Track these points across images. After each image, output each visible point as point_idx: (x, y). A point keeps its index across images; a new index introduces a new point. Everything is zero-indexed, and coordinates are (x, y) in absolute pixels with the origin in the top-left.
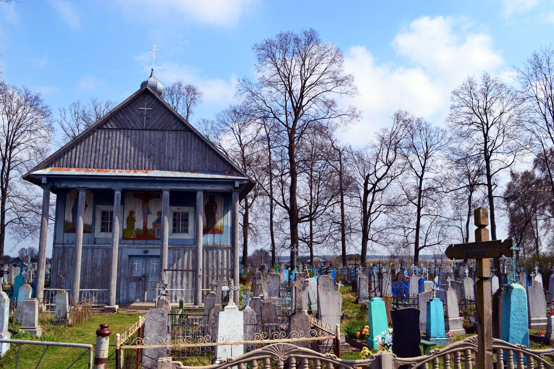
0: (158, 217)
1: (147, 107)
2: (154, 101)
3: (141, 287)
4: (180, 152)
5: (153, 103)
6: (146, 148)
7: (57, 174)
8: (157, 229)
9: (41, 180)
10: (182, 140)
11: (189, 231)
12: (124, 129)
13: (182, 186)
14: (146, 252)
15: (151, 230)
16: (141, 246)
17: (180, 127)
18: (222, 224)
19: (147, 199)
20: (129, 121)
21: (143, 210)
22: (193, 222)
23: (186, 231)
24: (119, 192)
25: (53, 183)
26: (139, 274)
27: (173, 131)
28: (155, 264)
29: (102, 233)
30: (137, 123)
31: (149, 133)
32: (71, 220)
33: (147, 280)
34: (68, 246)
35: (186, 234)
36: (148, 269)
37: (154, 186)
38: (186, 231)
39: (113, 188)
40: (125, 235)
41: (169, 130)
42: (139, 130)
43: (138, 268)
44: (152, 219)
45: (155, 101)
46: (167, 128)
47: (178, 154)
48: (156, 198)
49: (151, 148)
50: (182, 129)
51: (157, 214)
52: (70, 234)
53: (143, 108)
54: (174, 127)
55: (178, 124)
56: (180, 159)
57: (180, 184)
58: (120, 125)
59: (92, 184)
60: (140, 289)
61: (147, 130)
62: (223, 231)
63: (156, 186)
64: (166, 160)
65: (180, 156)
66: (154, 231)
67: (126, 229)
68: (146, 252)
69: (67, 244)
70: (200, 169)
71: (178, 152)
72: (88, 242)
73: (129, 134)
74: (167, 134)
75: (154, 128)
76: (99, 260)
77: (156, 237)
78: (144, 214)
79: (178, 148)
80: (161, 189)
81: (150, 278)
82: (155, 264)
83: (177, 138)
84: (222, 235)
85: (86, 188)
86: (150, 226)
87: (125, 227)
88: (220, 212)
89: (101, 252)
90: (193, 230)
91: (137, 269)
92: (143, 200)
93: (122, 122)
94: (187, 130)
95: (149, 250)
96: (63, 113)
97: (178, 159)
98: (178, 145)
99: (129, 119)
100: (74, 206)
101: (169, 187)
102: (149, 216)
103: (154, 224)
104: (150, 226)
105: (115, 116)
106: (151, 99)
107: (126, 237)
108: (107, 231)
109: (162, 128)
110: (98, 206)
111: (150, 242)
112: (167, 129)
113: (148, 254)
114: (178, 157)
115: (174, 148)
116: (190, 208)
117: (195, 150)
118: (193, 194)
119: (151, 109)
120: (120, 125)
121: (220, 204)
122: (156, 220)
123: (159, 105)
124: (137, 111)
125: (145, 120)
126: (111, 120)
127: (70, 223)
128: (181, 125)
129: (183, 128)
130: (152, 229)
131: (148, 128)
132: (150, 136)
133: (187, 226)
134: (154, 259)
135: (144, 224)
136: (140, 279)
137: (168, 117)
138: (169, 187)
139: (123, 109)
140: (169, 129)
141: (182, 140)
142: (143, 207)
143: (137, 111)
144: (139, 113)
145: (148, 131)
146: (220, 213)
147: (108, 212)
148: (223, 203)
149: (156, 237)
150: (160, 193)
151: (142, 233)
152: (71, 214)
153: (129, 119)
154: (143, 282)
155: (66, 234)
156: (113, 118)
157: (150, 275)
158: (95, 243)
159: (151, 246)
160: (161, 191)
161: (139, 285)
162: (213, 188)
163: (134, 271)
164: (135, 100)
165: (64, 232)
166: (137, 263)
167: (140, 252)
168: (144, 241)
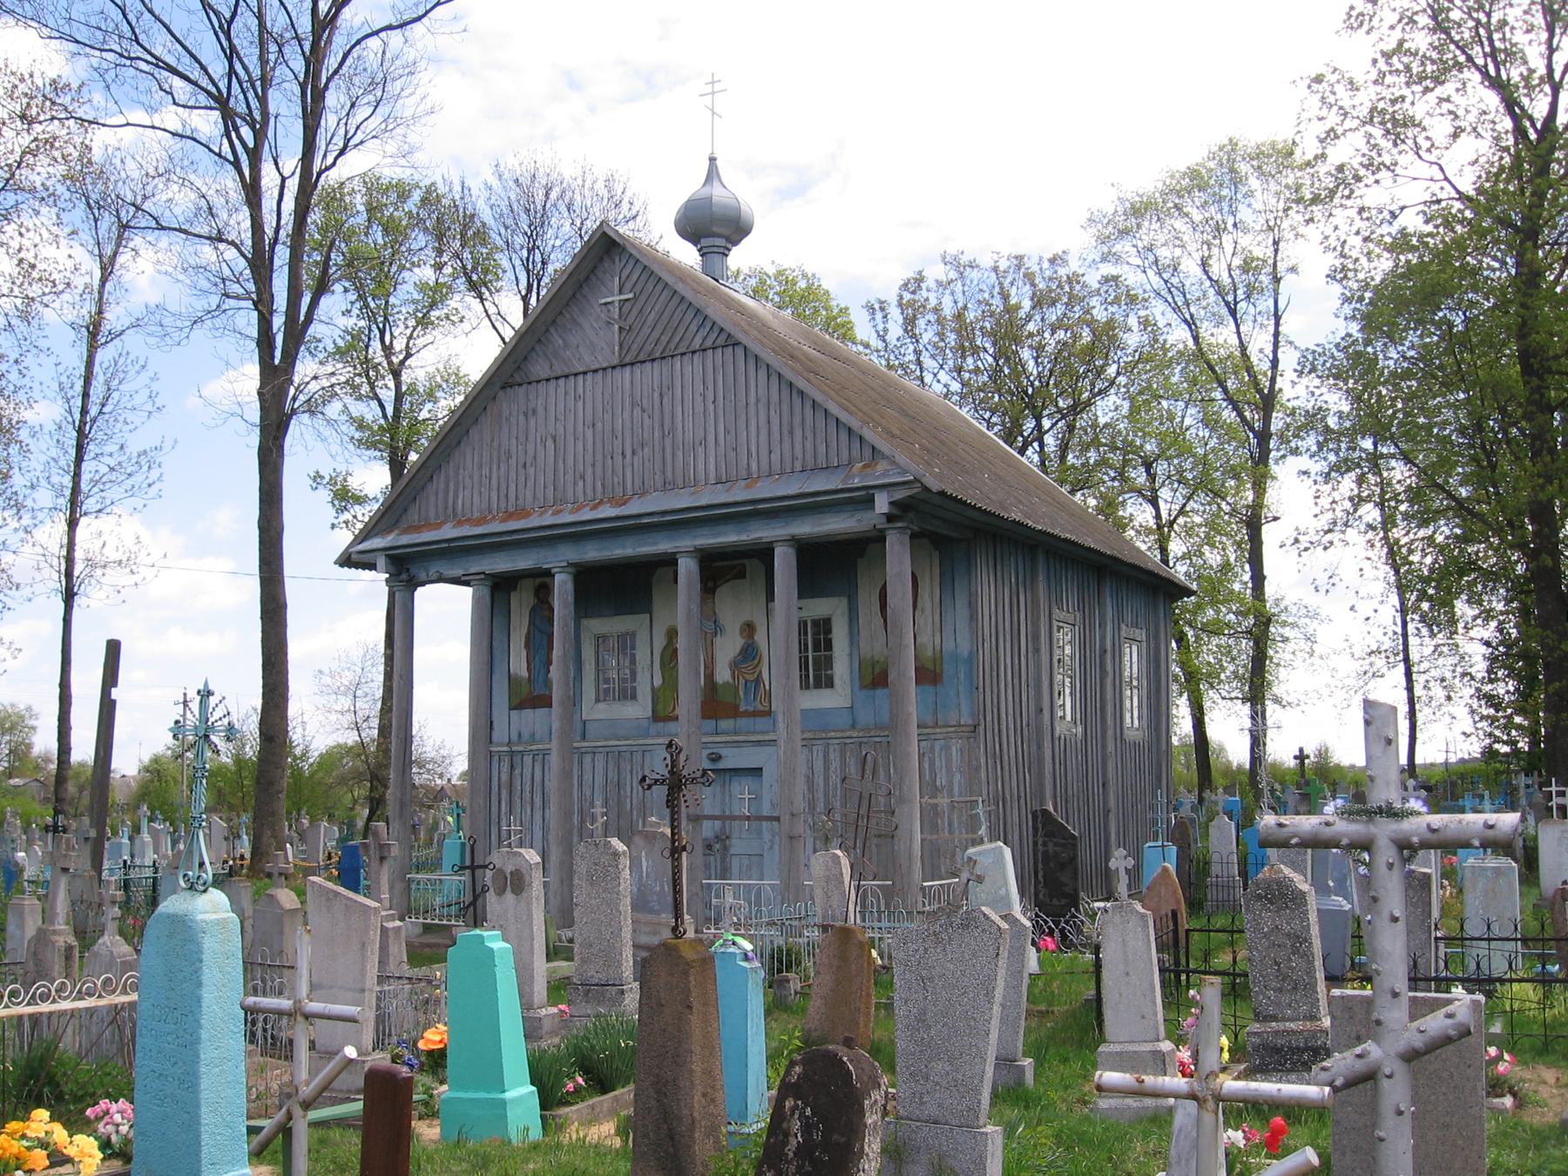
0: (743, 641)
8: (742, 681)
11: (837, 681)
14: (715, 758)
18: (938, 648)
22: (847, 651)
23: (830, 684)
28: (747, 796)
29: (601, 706)
34: (521, 748)
35: (825, 692)
37: (651, 545)
38: (830, 684)
39: (545, 566)
40: (660, 707)
48: (734, 578)
51: (742, 632)
53: (609, 300)
63: (656, 544)
67: (659, 689)
75: (641, 358)
77: (742, 708)
81: (734, 841)
82: (747, 796)
86: (723, 675)
87: (658, 682)
88: (928, 605)
90: (847, 677)
95: (723, 752)
96: (879, 316)
102: (718, 640)
103: (735, 666)
105: (691, 308)
107: (662, 714)
110: (584, 622)
111: (725, 724)
113: (721, 765)
116: (834, 601)
118: (764, 554)
121: (928, 582)
122: (740, 653)
131: (627, 360)
140: (683, 350)
146: (928, 611)
148: (937, 571)
149: (742, 708)
150: (546, 580)
154: (718, 857)
155: (514, 713)
158: (584, 737)
159: (728, 738)
160: (670, 561)
162: (744, 537)
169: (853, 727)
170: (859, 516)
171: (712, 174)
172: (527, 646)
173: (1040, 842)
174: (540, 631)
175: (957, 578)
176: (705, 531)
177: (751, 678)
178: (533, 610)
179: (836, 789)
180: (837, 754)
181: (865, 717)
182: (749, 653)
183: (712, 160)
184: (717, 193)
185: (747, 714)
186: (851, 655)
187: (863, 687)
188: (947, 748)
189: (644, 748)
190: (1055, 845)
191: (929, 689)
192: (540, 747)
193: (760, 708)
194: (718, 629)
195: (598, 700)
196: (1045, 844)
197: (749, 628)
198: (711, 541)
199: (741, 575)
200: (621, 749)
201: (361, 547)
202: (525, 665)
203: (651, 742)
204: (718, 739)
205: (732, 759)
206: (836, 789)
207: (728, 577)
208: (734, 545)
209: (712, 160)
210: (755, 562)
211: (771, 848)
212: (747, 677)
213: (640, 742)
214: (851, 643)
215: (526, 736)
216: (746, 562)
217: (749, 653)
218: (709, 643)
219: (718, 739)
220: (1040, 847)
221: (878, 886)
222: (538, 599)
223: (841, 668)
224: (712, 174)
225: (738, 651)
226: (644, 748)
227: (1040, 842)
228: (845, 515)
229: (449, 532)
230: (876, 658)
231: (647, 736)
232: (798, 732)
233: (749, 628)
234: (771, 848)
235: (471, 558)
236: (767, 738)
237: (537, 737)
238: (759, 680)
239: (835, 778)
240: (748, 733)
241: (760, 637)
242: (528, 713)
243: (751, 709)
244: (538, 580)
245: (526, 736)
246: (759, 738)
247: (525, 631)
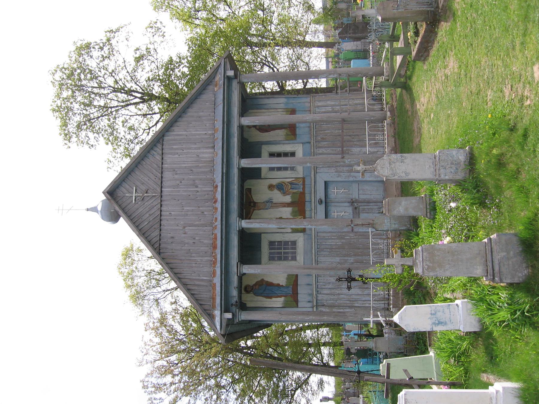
1: (133, 193)
2: (124, 184)
3: (366, 207)
4: (190, 148)
5: (127, 187)
6: (185, 191)
7: (219, 298)
8: (291, 190)
9: (229, 319)
10: (174, 147)
11: (292, 239)
12: (161, 220)
13: (234, 143)
15: (292, 197)
16: (313, 208)
17: (158, 150)
19: (252, 205)
20: (150, 215)
21: (267, 209)
22: (281, 145)
23: (294, 243)
24: (243, 221)
25: (232, 305)
26: (350, 210)
27: (162, 158)
28: (336, 191)
29: (298, 258)
30: (152, 204)
31: (165, 188)
32: (282, 299)
33: (356, 200)
36: (342, 200)
38: (294, 243)
41: (162, 164)
42: (161, 201)
43: (341, 212)
44: (278, 197)
45: (124, 183)
46: (159, 167)
47: (193, 151)
48: (251, 194)
49: (184, 185)
50: (160, 148)
51: (272, 190)
52: (299, 292)
53: (134, 198)
54: (158, 158)
55: (154, 153)
56: (199, 148)
57: (231, 145)
58: (155, 226)
59: (232, 255)
60: (368, 209)
61: (161, 191)
62: (292, 109)
64: (200, 165)
65: (195, 149)
66: (294, 193)
68: (321, 202)
69: (312, 302)
70: (211, 122)
71: (190, 151)
72: (308, 285)
73: (168, 213)
74: (166, 166)
75: (159, 183)
76: (332, 260)
77: (301, 190)
78: (272, 207)
79: (185, 151)
80: (238, 168)
81: (354, 197)
82: (336, 191)
83: (171, 154)
84: (297, 110)
85: (237, 263)
86: (288, 199)
89: (322, 258)
90: (291, 145)
91: (343, 214)
92: (254, 210)
93: (151, 223)
94: (161, 141)
97: (199, 151)
98: (182, 151)
99: (147, 215)
100: (263, 296)
101: (236, 159)
103: (285, 193)
104: (288, 199)
105: (143, 232)
106: (122, 189)
108: (295, 253)
109: (159, 173)
111: (307, 198)
112: (161, 166)
113: (323, 199)
114: (196, 151)
115: (185, 156)
117: (187, 130)
119: (134, 188)
120: (155, 226)
122: (280, 191)
123: (130, 178)
124: (136, 206)
125: (149, 195)
126: (148, 238)
127: (285, 301)
128: (156, 149)
129: (159, 146)
130: (291, 197)
132: (169, 187)
133: (286, 243)
134: (329, 192)
135: (285, 207)
136: (356, 208)
137: (145, 166)
138: (236, 159)
139: (131, 220)
140: (161, 163)
141: (174, 147)
142: (263, 209)
143: (136, 206)
144: (139, 203)
145: (163, 189)
147: (270, 253)
149: (301, 190)
151: (296, 209)
152: (274, 299)
153: (147, 215)
154: (360, 204)
156: (146, 235)
157: (351, 196)
159: (313, 195)
161: (364, 209)
162: (236, 135)
163: (346, 217)
164: (120, 206)
165: (297, 307)
166: (335, 212)
167: (321, 209)
168: (307, 204)
169: (310, 143)
170: (233, 89)
171: (94, 209)
172: (270, 297)
173: (349, 35)
174: (264, 290)
175: (259, 103)
176: (232, 152)
177: (290, 186)
178: (256, 294)
179: (333, 150)
180: (320, 149)
181: (306, 139)
182: (280, 187)
183: (88, 210)
184: (99, 208)
185: (304, 188)
186: (283, 144)
187: (295, 139)
188: (318, 107)
189: (316, 236)
190: (350, 30)
191: (297, 112)
192: (314, 290)
193: (301, 182)
194: (270, 201)
195: (295, 260)
196: (350, 34)
197: (271, 187)
198: (236, 149)
199: (250, 190)
200: (316, 248)
201: (218, 327)
202: (279, 299)
203: (313, 232)
204: (313, 200)
205: (321, 194)
206: (333, 150)
207: (250, 196)
208: (238, 141)
209: (88, 210)
210: (245, 184)
211: (355, 177)
212: (289, 189)
213: (314, 237)
214: (279, 144)
215: (310, 298)
216: (245, 187)
217: (280, 187)
218: (275, 205)
219: (313, 200)
220: (351, 35)
221: (372, 252)
222: (251, 291)
223: (288, 148)
224: (94, 209)
225: (279, 192)
226: (316, 236)
227: (349, 35)
228: (233, 94)
229: (217, 280)
230: (285, 134)
231: (311, 235)
232: (311, 157)
233: (271, 187)
234: (355, 177)
235: (230, 270)
236: (313, 178)
237: (310, 292)
238: (291, 183)
239: (329, 150)
240: (311, 187)
241: (274, 182)
242: (300, 297)
243: (302, 186)
244: (243, 291)
245: (310, 298)
246: (313, 181)
247: (264, 299)
